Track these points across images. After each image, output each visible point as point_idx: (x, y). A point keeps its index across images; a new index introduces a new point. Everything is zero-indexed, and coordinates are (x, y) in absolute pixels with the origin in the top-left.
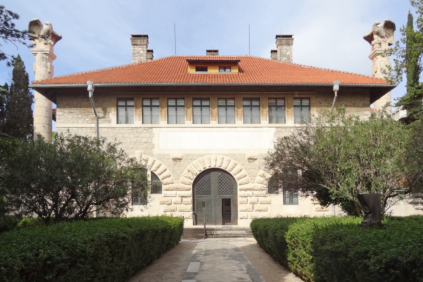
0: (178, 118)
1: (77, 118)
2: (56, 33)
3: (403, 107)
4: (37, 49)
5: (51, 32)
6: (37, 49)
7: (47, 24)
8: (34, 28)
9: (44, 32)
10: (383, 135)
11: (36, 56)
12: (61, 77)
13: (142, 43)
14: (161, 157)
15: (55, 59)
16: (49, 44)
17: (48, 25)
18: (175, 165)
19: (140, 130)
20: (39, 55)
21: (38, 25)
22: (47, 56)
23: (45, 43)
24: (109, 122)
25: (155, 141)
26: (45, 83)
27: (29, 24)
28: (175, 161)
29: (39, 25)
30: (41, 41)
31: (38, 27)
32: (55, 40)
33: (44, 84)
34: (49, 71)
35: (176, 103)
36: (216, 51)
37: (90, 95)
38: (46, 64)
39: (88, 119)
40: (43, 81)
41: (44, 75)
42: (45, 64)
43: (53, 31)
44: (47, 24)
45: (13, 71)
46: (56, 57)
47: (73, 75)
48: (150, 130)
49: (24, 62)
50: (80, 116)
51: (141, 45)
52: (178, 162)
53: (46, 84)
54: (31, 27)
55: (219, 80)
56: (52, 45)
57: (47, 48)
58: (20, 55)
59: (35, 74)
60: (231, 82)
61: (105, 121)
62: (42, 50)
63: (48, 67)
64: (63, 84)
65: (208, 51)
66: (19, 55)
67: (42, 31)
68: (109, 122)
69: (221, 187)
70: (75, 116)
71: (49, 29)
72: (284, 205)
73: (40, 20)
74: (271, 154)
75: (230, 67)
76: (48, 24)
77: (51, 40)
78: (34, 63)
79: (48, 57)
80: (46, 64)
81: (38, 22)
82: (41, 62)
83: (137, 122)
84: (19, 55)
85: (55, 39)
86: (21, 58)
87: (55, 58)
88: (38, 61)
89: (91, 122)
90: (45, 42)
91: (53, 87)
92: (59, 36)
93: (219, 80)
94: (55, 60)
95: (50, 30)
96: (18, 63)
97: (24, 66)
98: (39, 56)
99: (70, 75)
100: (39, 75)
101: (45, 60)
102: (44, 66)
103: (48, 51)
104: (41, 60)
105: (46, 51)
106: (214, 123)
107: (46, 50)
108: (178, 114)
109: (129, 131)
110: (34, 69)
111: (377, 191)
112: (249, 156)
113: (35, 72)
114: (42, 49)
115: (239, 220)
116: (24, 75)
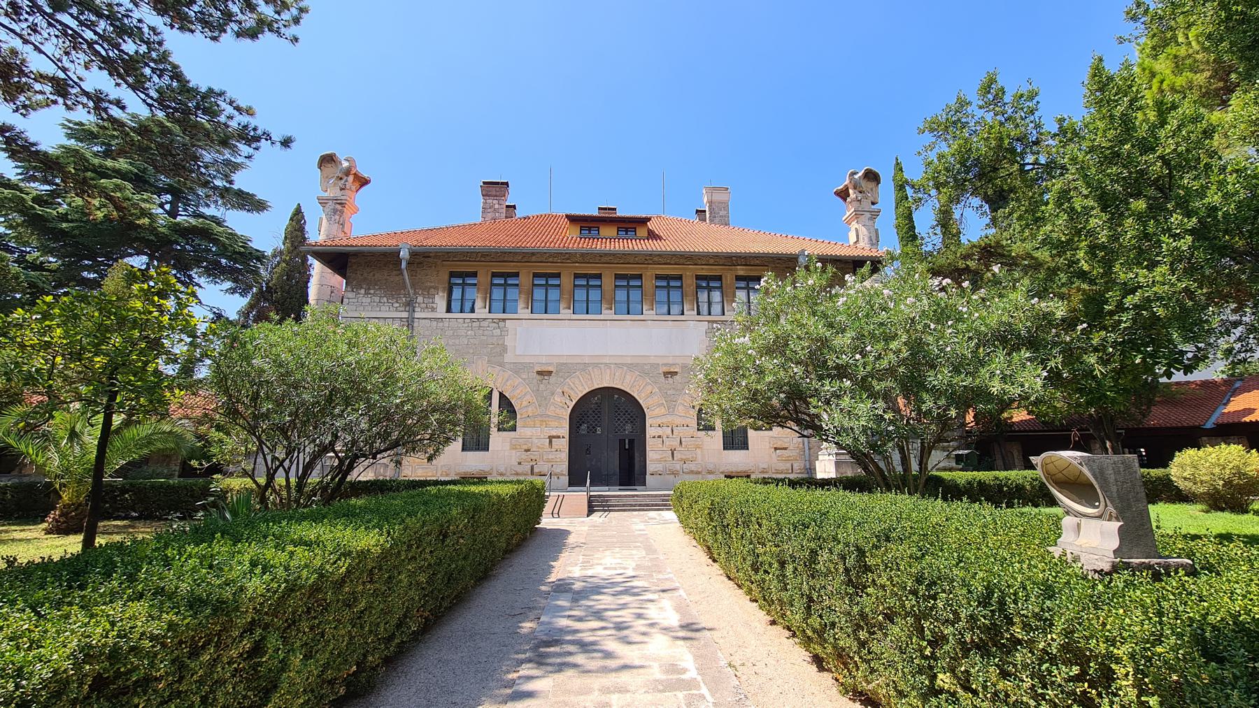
0: (534, 303)
1: (380, 302)
3: (1121, 526)
10: (12, 658)
13: (498, 194)
14: (518, 369)
18: (541, 381)
19: (485, 324)
24: (433, 310)
25: (508, 341)
28: (542, 375)
31: (333, 164)
35: (588, 282)
36: (615, 209)
37: (404, 265)
39: (398, 305)
48: (502, 324)
50: (385, 299)
51: (496, 196)
52: (546, 377)
55: (617, 245)
60: (636, 249)
61: (427, 307)
65: (599, 209)
66: (299, 204)
68: (433, 310)
69: (619, 420)
70: (377, 299)
72: (726, 451)
75: (635, 228)
83: (481, 312)
89: (403, 309)
93: (617, 245)
106: (648, 313)
108: (508, 297)
109: (466, 325)
112: (666, 369)
115: (648, 477)
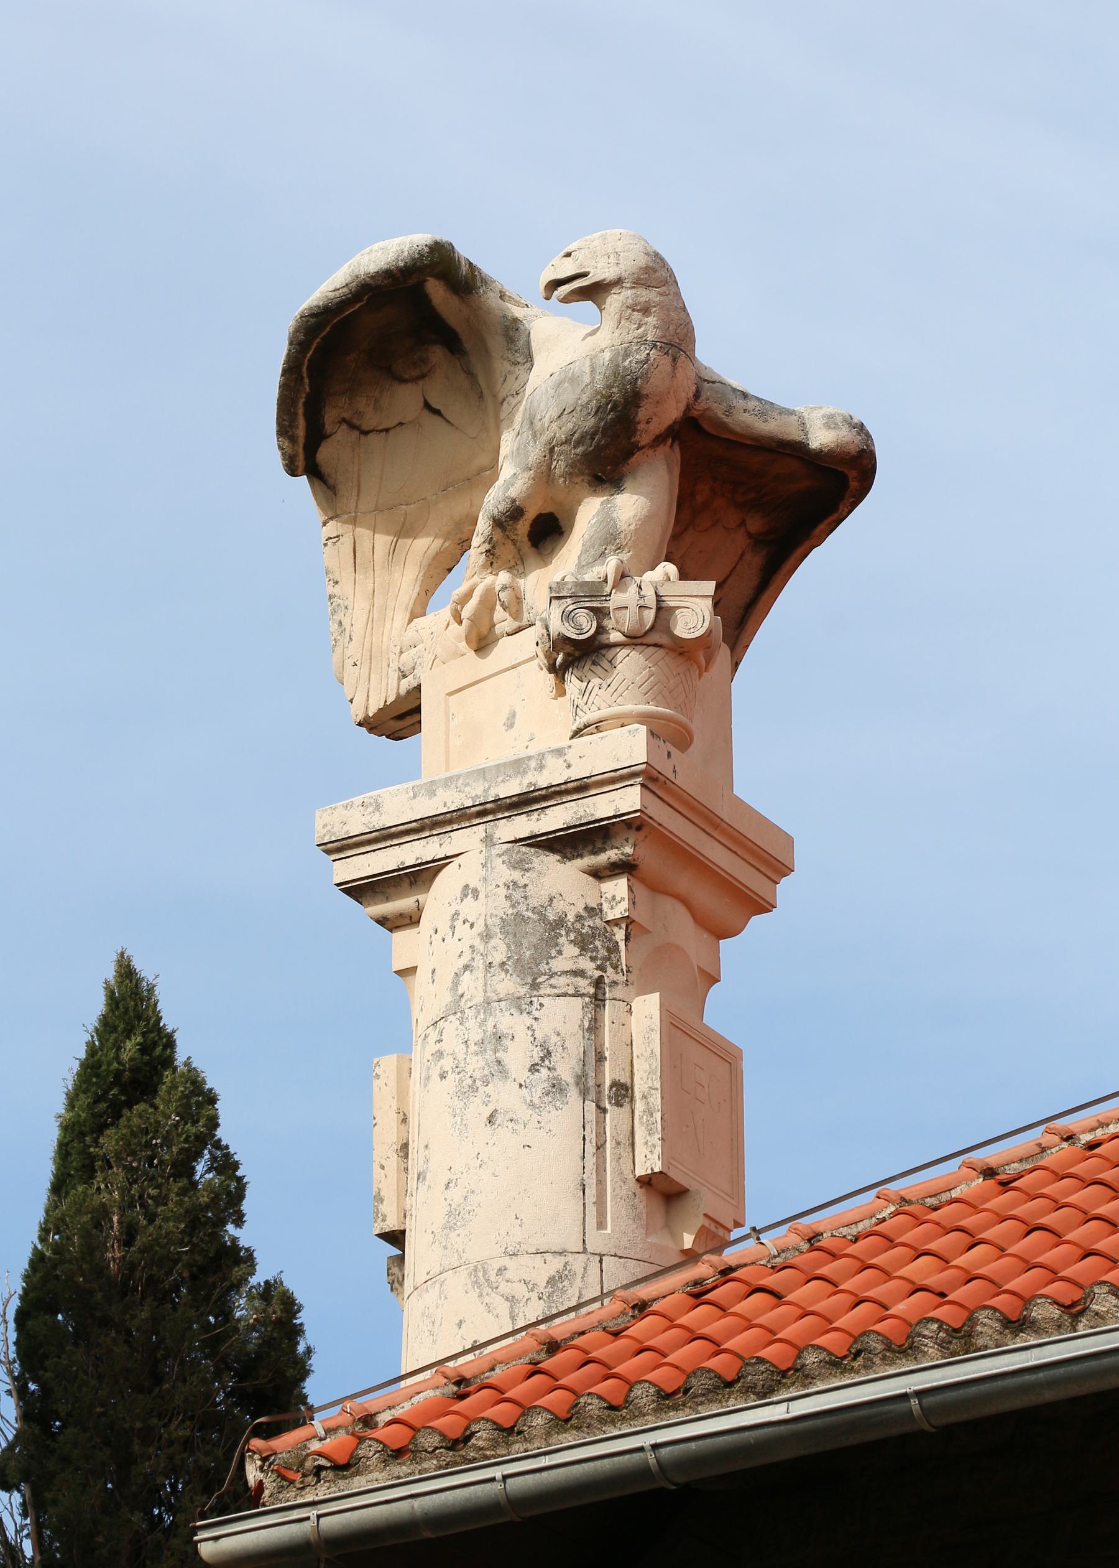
2: (767, 408)
4: (431, 789)
5: (673, 412)
6: (431, 789)
7: (595, 292)
8: (370, 420)
9: (535, 453)
11: (411, 920)
12: (813, 1238)
15: (763, 906)
16: (634, 640)
17: (615, 301)
20: (469, 892)
21: (437, 354)
22: (598, 874)
23: (561, 642)
26: (502, 1412)
27: (291, 370)
29: (452, 342)
30: (503, 620)
32: (757, 541)
33: (483, 1436)
34: (648, 1161)
38: (594, 1027)
40: (462, 1386)
41: (555, 1264)
42: (576, 1044)
43: (704, 383)
44: (595, 292)
45: (22, 1318)
46: (779, 868)
47: (1060, 1153)
49: (211, 1082)
53: (508, 1432)
54: (330, 416)
56: (682, 650)
57: (596, 726)
58: (145, 968)
59: (396, 1283)
62: (512, 788)
63: (623, 1092)
64: (836, 1364)
66: (126, 972)
67: (508, 442)
71: (616, 373)
73: (467, 250)
74: (478, 1288)
76: (601, 271)
77: (671, 569)
78: (387, 1064)
79: (619, 887)
80: (594, 1027)
81: (436, 290)
82: (510, 1021)
84: (126, 972)
85: (755, 524)
86: (169, 1020)
87: (751, 879)
88: (455, 1009)
90: (558, 626)
91: (642, 1473)
92: (820, 438)
94: (757, 921)
95: (656, 383)
96: (110, 1142)
97: (226, 1165)
98: (471, 909)
99: (988, 1155)
100: (458, 1282)
101: (568, 956)
102: (556, 1088)
103: (617, 778)
104: (508, 985)
105: (581, 788)
107: (578, 772)
110: (386, 1181)
111: (65, 1168)
113: (396, 1238)
114: (518, 766)
116: (213, 1343)
